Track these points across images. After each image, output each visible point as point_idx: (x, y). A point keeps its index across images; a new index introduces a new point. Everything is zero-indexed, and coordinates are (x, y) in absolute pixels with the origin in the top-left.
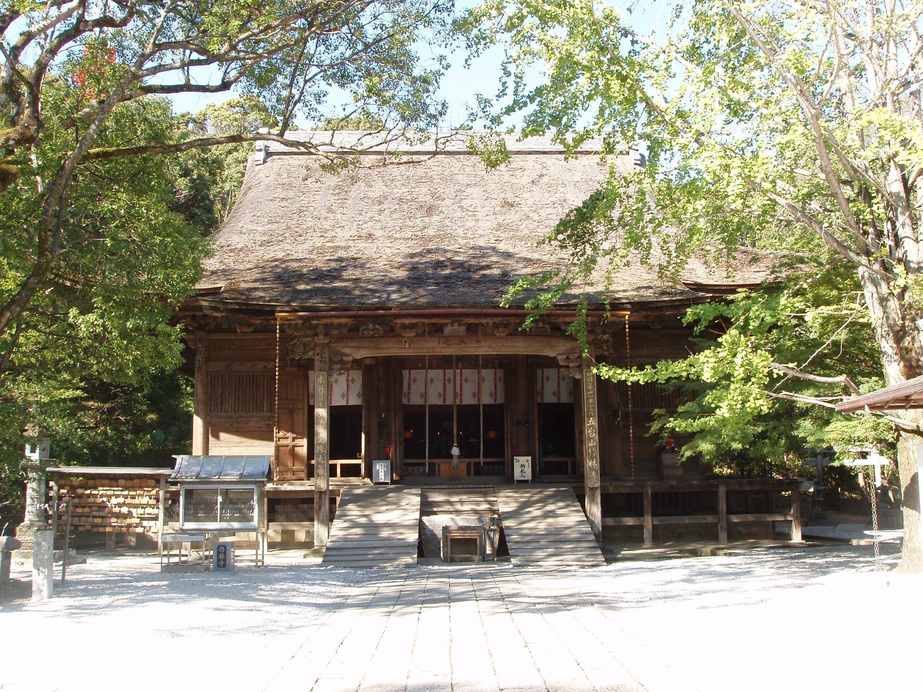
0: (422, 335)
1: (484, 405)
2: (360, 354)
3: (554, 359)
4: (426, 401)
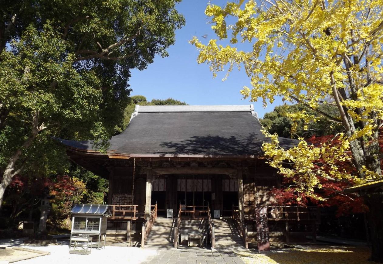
0: (184, 167)
1: (204, 192)
2: (162, 173)
3: (228, 176)
4: (203, 190)
